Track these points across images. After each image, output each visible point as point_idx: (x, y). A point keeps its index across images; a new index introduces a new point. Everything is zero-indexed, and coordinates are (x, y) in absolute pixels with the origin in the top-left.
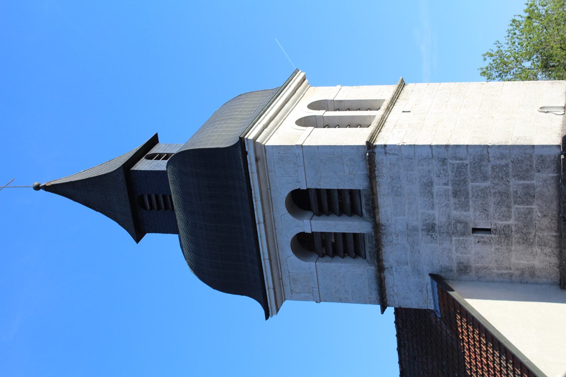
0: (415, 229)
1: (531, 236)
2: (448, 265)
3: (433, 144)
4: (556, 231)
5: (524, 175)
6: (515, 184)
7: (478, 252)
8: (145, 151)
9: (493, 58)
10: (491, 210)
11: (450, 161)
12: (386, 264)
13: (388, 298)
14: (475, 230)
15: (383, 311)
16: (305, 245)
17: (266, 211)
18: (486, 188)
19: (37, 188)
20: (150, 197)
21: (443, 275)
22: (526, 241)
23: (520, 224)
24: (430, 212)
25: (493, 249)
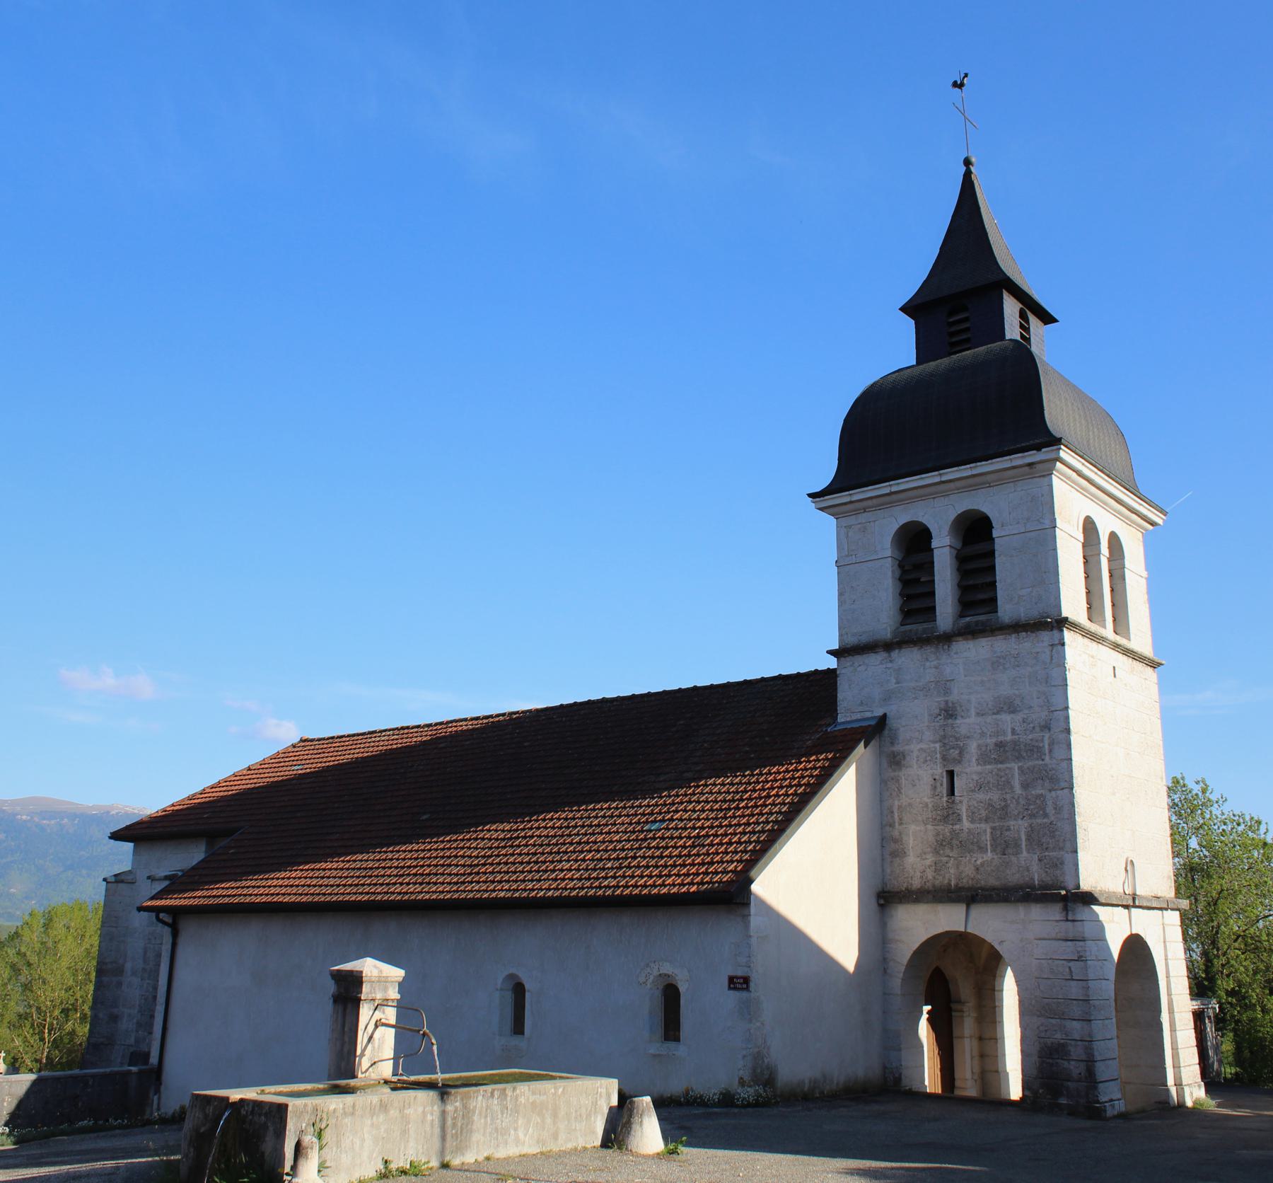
0: (947, 691)
1: (948, 851)
3: (1070, 712)
4: (956, 885)
5: (1034, 839)
6: (1020, 827)
7: (920, 779)
10: (981, 796)
11: (1047, 736)
12: (895, 654)
14: (951, 774)
15: (830, 652)
16: (914, 541)
17: (958, 484)
18: (1012, 787)
19: (967, 162)
20: (966, 319)
21: (886, 732)
22: (941, 845)
23: (964, 836)
24: (973, 712)
25: (926, 799)
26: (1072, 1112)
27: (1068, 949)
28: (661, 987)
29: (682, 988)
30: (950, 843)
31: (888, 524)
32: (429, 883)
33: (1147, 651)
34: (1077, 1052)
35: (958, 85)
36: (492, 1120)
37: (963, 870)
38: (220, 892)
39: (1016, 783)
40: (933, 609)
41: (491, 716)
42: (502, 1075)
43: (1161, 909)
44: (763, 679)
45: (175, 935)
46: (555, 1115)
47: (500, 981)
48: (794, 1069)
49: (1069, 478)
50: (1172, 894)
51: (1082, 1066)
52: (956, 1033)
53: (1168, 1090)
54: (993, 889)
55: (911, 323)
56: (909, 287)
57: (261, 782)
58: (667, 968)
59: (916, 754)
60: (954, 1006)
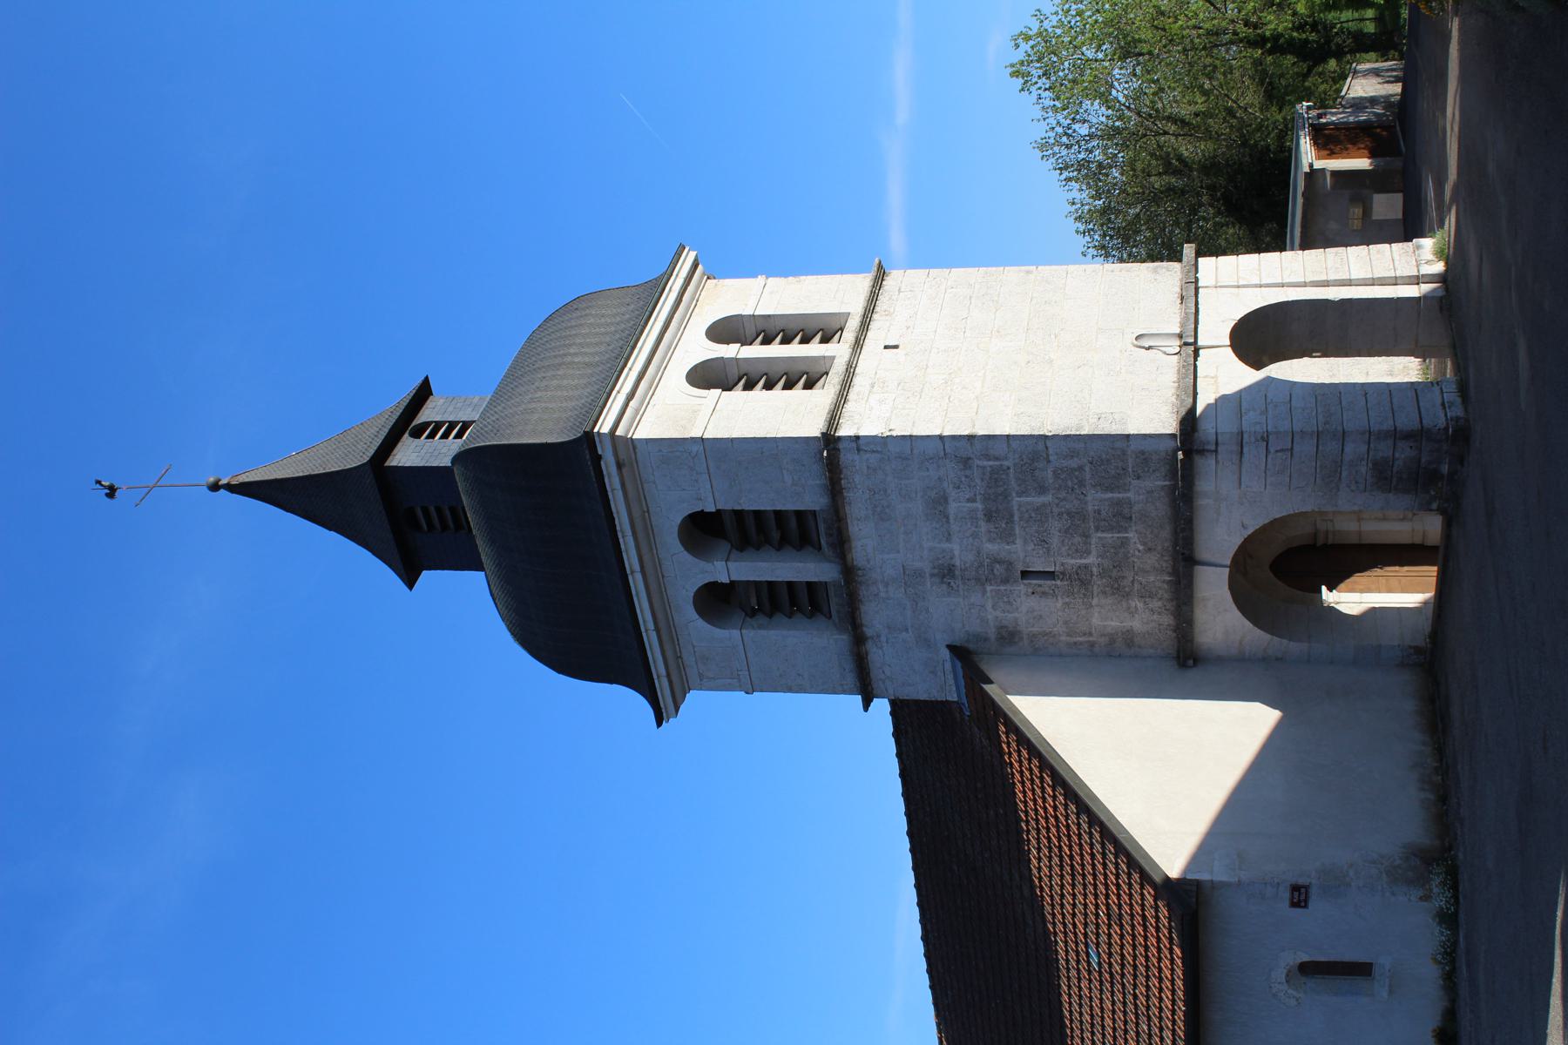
0: (919, 574)
1: (1126, 582)
3: (946, 433)
4: (1170, 574)
6: (1095, 499)
7: (1029, 609)
8: (407, 422)
9: (1031, 43)
10: (1055, 541)
12: (869, 632)
14: (1025, 574)
15: (866, 707)
16: (717, 601)
17: (644, 550)
18: (1044, 505)
19: (215, 487)
20: (425, 511)
21: (971, 646)
22: (1117, 589)
23: (1107, 563)
24: (946, 545)
25: (1059, 605)
27: (1253, 453)
28: (1303, 979)
29: (1306, 958)
30: (1116, 580)
31: (696, 629)
33: (864, 282)
34: (1384, 449)
35: (112, 492)
37: (1151, 566)
39: (1040, 500)
40: (810, 586)
43: (1197, 289)
44: (899, 755)
50: (1176, 265)
51: (1400, 444)
52: (1355, 541)
54: (1175, 533)
55: (426, 576)
56: (383, 575)
58: (1280, 974)
59: (998, 613)
60: (1320, 542)
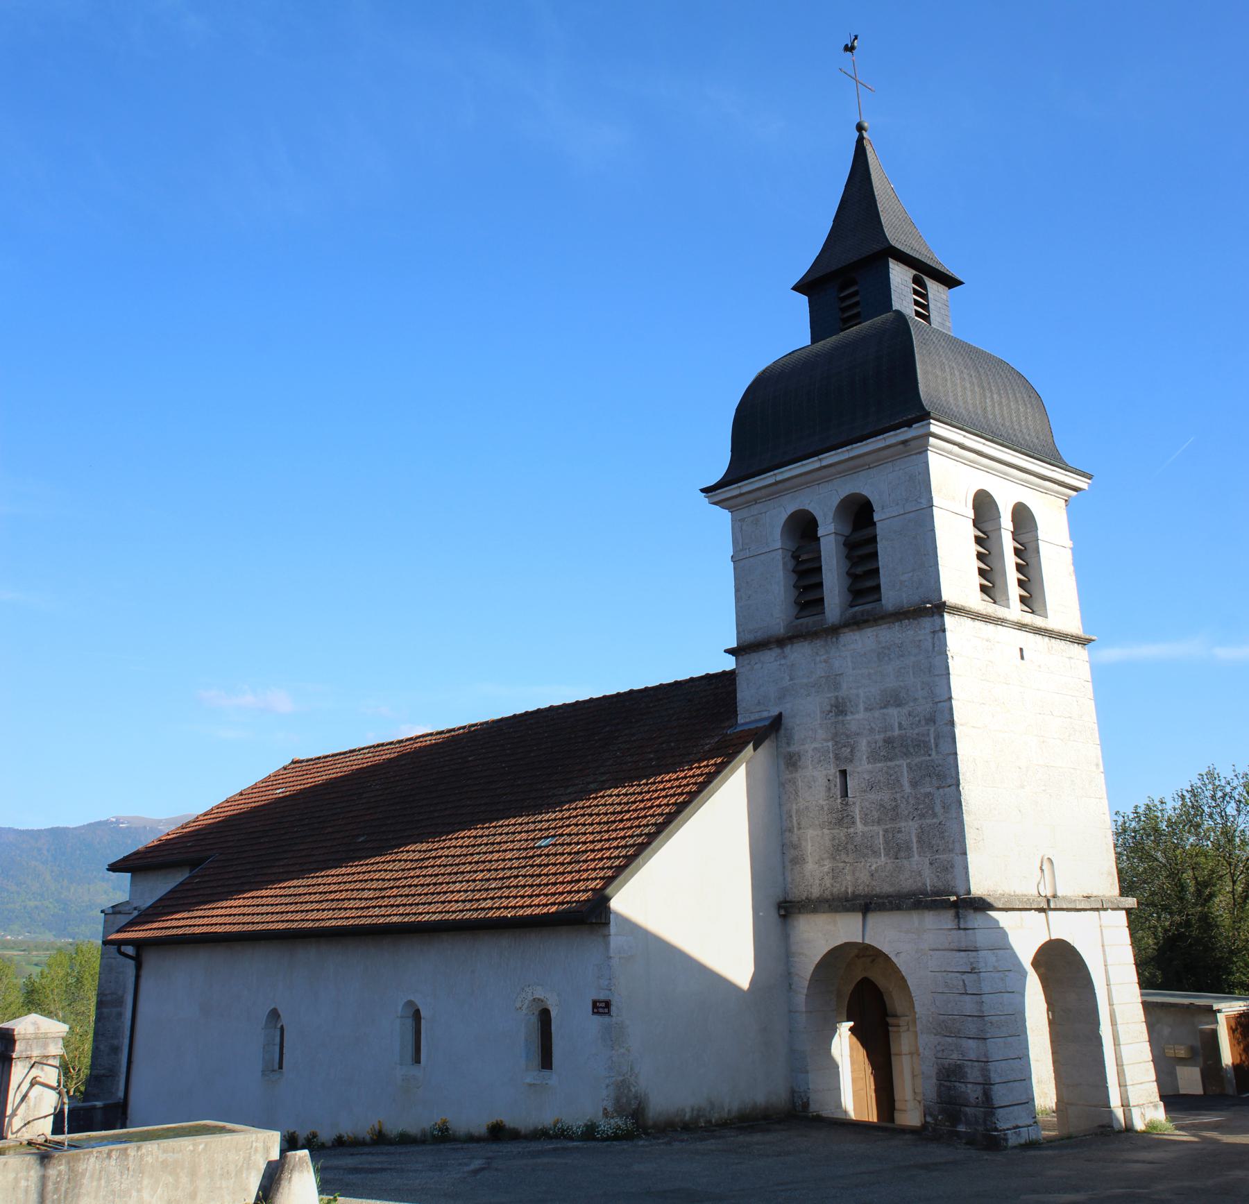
0: (837, 687)
1: (844, 857)
2: (796, 738)
5: (925, 842)
6: (910, 828)
10: (872, 796)
11: (932, 730)
12: (788, 649)
13: (746, 657)
14: (844, 773)
15: (728, 651)
16: (803, 528)
19: (860, 128)
20: (855, 294)
21: (782, 732)
22: (837, 849)
23: (858, 840)
24: (861, 707)
25: (821, 802)
26: (971, 1141)
27: (960, 961)
28: (537, 1013)
29: (553, 1014)
31: (778, 514)
32: (539, 885)
33: (1075, 628)
34: (973, 1074)
35: (849, 48)
36: (108, 1182)
37: (861, 876)
38: (175, 923)
39: (905, 782)
41: (453, 730)
42: (182, 1128)
45: (139, 967)
46: (193, 1174)
47: (400, 1009)
48: (668, 1095)
49: (950, 453)
50: (1116, 891)
52: (894, 1050)
53: (1111, 1112)
55: (805, 299)
57: (245, 807)
58: (540, 993)
59: (810, 753)
60: (890, 1020)
